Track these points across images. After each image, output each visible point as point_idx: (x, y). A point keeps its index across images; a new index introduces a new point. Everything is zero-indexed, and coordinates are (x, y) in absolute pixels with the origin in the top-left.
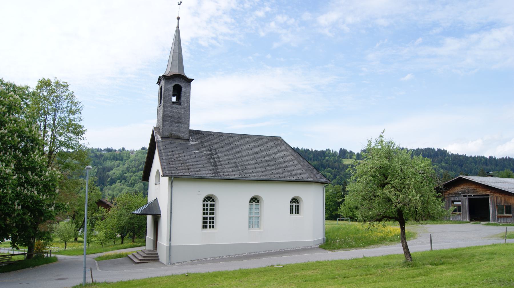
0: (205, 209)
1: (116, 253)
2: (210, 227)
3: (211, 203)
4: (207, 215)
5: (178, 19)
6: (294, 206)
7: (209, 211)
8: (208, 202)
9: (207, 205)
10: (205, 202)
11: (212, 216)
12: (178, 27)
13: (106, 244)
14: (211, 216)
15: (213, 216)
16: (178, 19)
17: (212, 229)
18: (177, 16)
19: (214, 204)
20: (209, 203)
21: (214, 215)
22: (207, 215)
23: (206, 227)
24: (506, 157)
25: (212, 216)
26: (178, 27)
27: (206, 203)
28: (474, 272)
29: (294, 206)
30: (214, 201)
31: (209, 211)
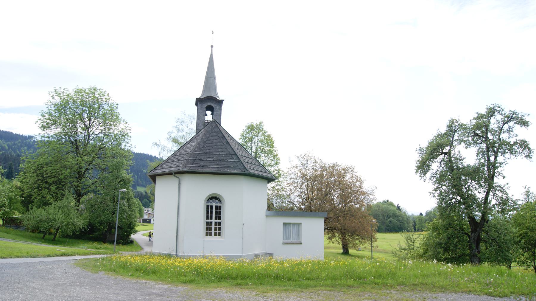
0: (209, 214)
1: (148, 263)
2: (215, 235)
3: (217, 205)
4: (212, 219)
5: (212, 46)
6: (214, 208)
7: (214, 215)
8: (212, 203)
9: (212, 207)
10: (209, 203)
11: (218, 221)
12: (211, 54)
13: (443, 164)
14: (211, 220)
15: (219, 221)
16: (212, 46)
17: (217, 237)
18: (211, 44)
19: (221, 206)
20: (214, 205)
21: (220, 219)
22: (212, 219)
23: (211, 235)
24: (415, 169)
25: (209, 220)
26: (211, 54)
27: (210, 204)
28: (319, 180)
29: (214, 208)
30: (220, 201)
31: (214, 215)
